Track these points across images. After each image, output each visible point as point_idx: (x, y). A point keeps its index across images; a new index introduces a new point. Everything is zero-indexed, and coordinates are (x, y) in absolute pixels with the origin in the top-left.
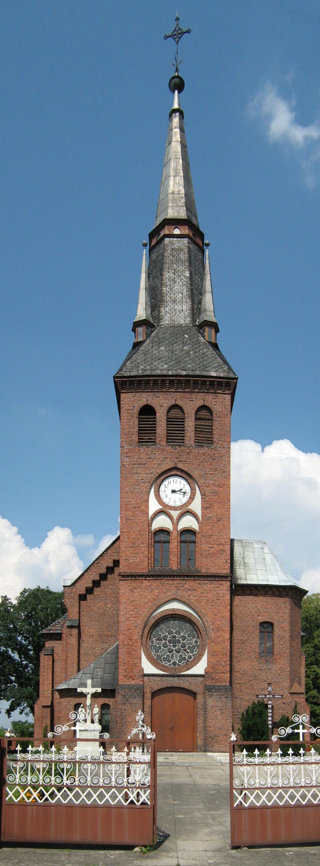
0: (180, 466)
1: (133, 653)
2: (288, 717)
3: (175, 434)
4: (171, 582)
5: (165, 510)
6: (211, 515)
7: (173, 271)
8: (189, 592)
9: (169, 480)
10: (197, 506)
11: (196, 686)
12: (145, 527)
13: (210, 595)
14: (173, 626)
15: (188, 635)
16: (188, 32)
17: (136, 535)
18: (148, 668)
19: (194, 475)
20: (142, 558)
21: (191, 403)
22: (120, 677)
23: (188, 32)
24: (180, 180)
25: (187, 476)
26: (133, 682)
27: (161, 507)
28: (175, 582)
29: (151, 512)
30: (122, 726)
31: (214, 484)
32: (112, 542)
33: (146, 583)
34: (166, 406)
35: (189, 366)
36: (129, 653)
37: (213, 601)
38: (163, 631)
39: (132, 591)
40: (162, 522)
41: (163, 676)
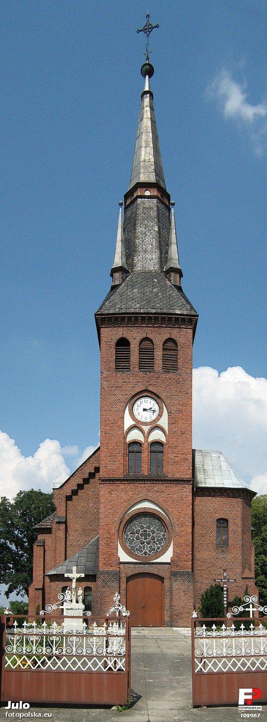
0: (150, 388)
3: (146, 363)
4: (142, 485)
6: (176, 429)
9: (141, 400)
10: (164, 422)
11: (164, 572)
13: (175, 496)
15: (157, 529)
16: (157, 26)
17: (114, 446)
21: (159, 336)
23: (157, 26)
24: (150, 150)
25: (156, 397)
26: (111, 569)
29: (126, 427)
33: (122, 486)
36: (108, 544)
38: (136, 526)
39: (110, 493)
41: (136, 563)
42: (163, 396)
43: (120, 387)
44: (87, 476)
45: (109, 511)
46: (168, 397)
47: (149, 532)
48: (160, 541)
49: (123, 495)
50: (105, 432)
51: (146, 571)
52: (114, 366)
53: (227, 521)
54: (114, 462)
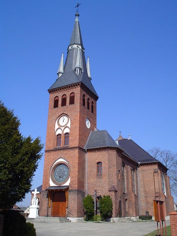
3: (64, 103)
8: (65, 155)
10: (69, 125)
12: (53, 134)
14: (61, 167)
16: (76, 7)
19: (68, 115)
23: (76, 7)
25: (66, 115)
33: (52, 153)
34: (62, 95)
38: (58, 170)
40: (59, 132)
41: (57, 186)
53: (100, 162)
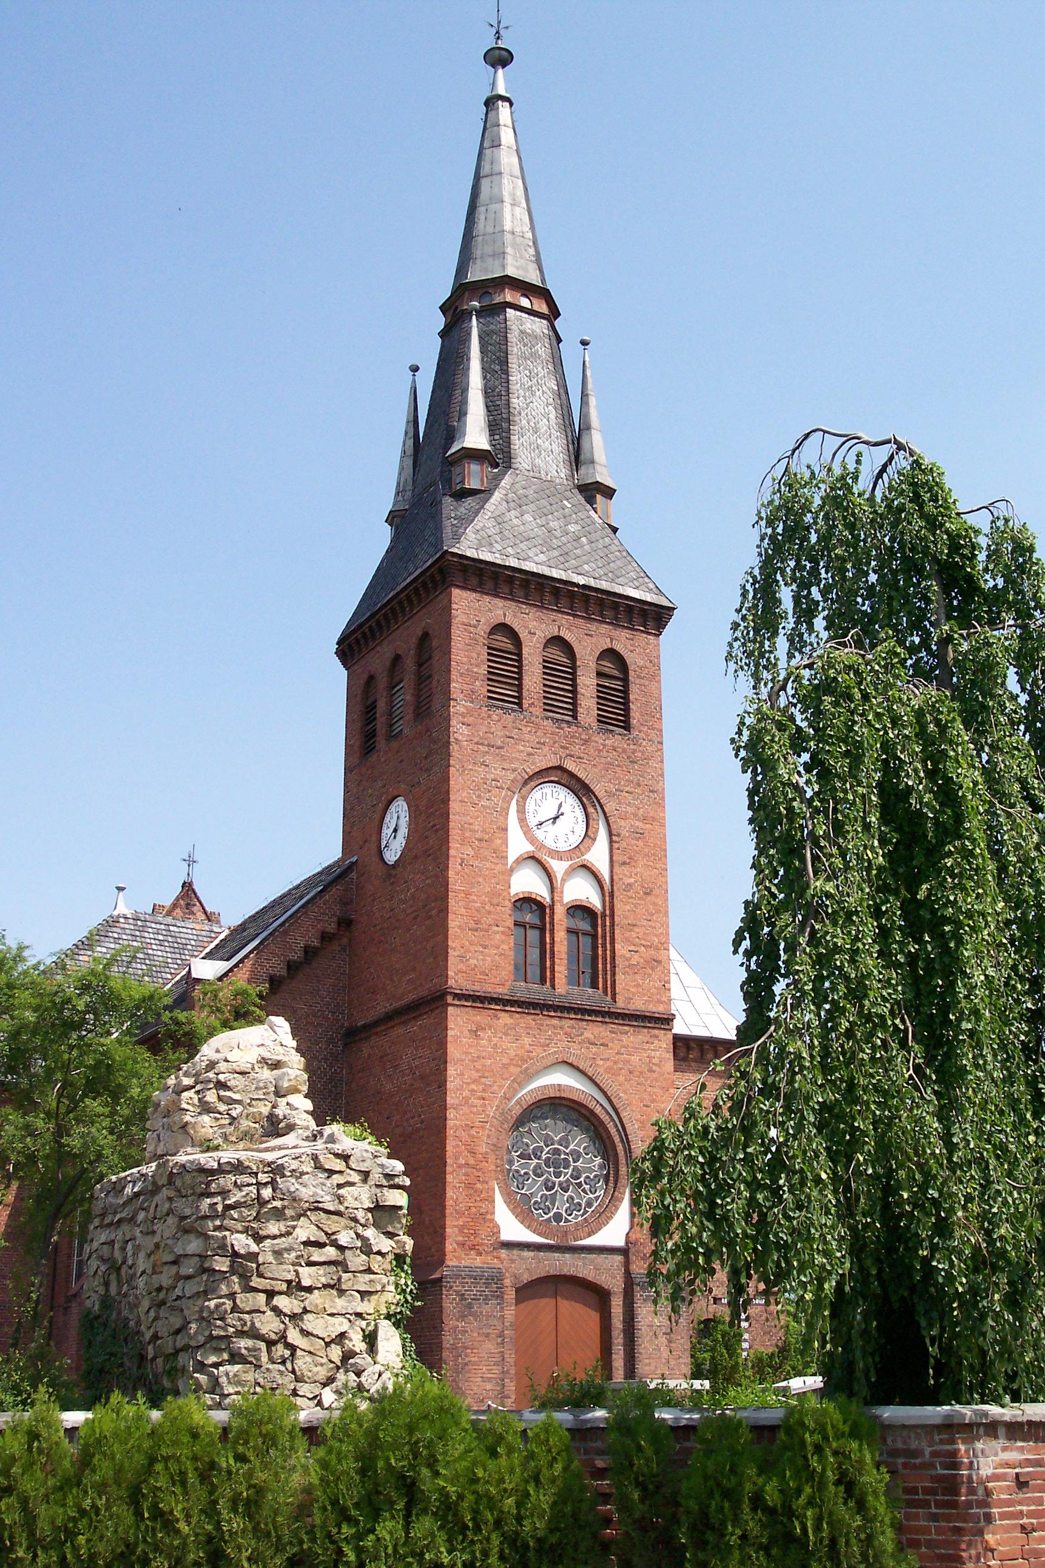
0: (570, 765)
1: (479, 1186)
2: (201, 1484)
4: (555, 1022)
5: (538, 855)
6: (632, 880)
7: (527, 372)
8: (594, 1049)
9: (544, 791)
11: (608, 1275)
13: (635, 1059)
15: (585, 1148)
17: (484, 903)
18: (511, 1227)
20: (497, 957)
21: (590, 640)
22: (449, 1247)
24: (521, 212)
25: (581, 789)
26: (478, 1261)
27: (531, 848)
28: (564, 1022)
29: (512, 857)
30: (458, 1373)
31: (635, 815)
32: (83, 933)
33: (505, 1019)
35: (586, 567)
36: (469, 1186)
37: (641, 1073)
39: (474, 1033)
41: (538, 1247)
42: (598, 789)
43: (499, 748)
44: (296, 956)
45: (473, 1086)
46: (610, 794)
47: (567, 1154)
48: (592, 1183)
49: (506, 1043)
50: (463, 859)
51: (552, 1272)
52: (484, 691)
54: (485, 947)
